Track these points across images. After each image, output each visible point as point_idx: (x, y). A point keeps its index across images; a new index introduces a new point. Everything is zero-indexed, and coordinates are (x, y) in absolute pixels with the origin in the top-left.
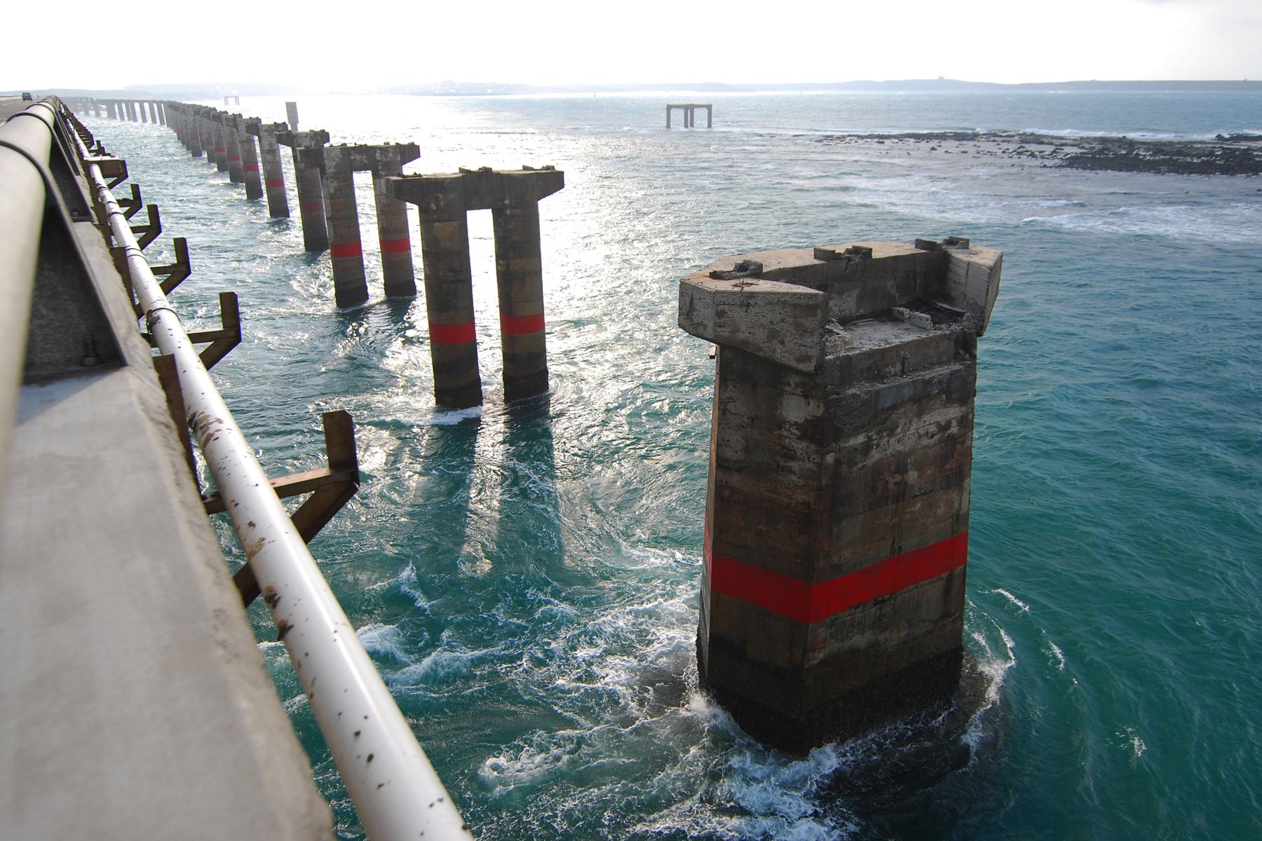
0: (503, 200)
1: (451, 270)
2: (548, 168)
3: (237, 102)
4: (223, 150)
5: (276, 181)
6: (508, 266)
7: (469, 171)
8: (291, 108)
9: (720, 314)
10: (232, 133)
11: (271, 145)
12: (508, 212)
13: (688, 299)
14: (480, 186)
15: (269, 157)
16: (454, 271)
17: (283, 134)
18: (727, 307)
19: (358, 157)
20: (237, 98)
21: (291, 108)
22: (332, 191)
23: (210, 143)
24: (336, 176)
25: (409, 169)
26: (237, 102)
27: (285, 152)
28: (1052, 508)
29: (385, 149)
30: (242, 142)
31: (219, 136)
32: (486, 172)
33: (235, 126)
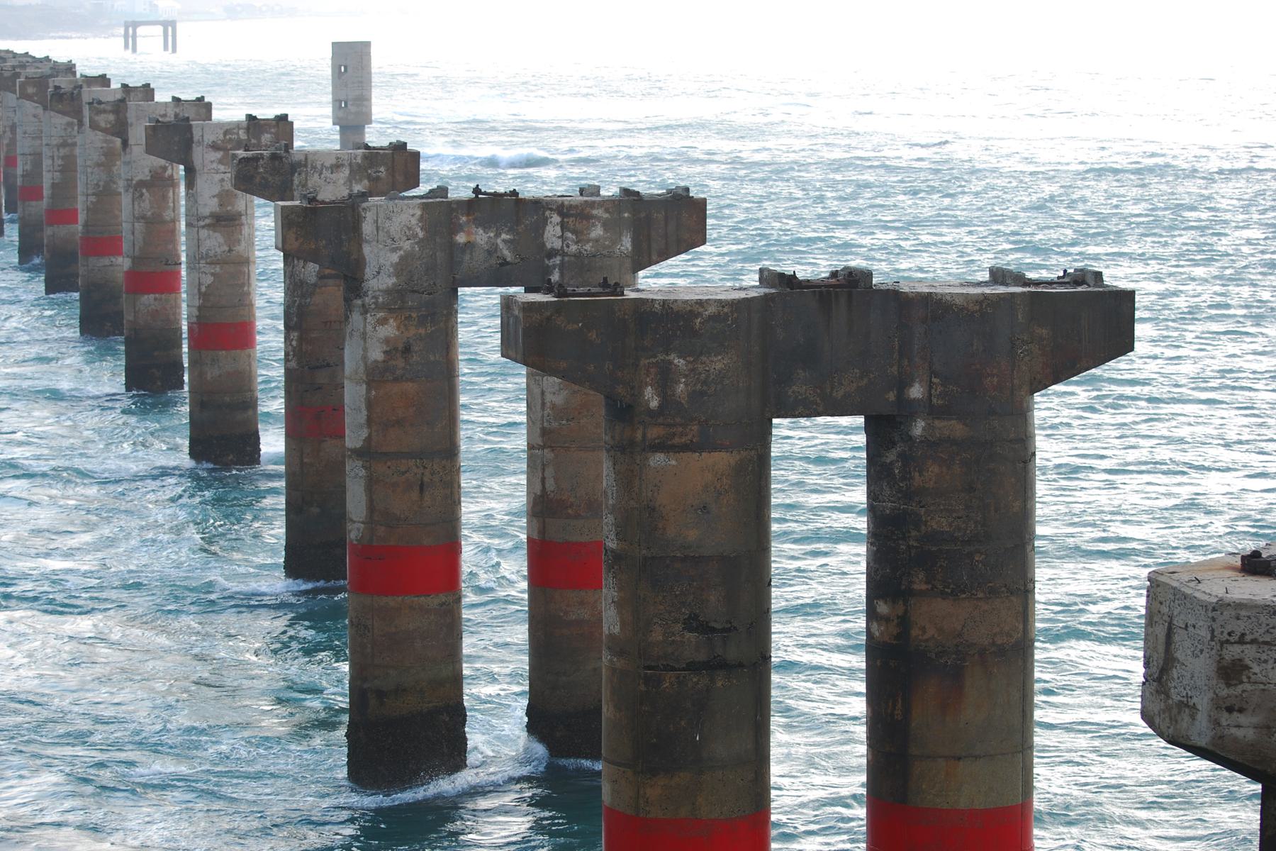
0: (902, 384)
1: (696, 624)
2: (1080, 277)
3: (170, 42)
4: (71, 216)
5: (226, 330)
6: (904, 622)
7: (789, 281)
8: (351, 65)
9: (1231, 672)
10: (109, 156)
11: (224, 197)
12: (918, 428)
13: (1161, 631)
14: (837, 333)
15: (214, 242)
16: (704, 628)
17: (265, 155)
18: (1249, 652)
19: (481, 237)
20: (169, 26)
21: (351, 65)
22: (377, 354)
23: (33, 192)
24: (396, 303)
25: (660, 280)
26: (170, 42)
27: (264, 221)
28: (490, 823)
29: (577, 211)
30: (138, 188)
31: (68, 167)
32: (852, 284)
33: (120, 129)
